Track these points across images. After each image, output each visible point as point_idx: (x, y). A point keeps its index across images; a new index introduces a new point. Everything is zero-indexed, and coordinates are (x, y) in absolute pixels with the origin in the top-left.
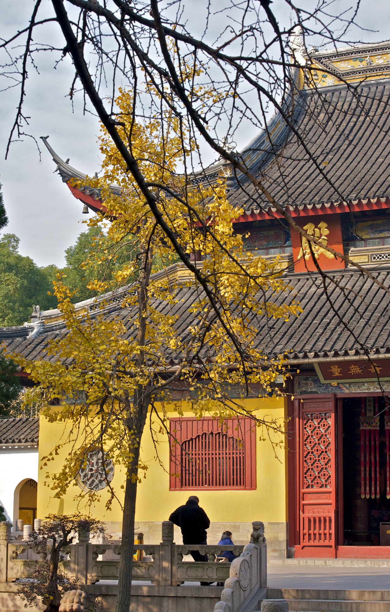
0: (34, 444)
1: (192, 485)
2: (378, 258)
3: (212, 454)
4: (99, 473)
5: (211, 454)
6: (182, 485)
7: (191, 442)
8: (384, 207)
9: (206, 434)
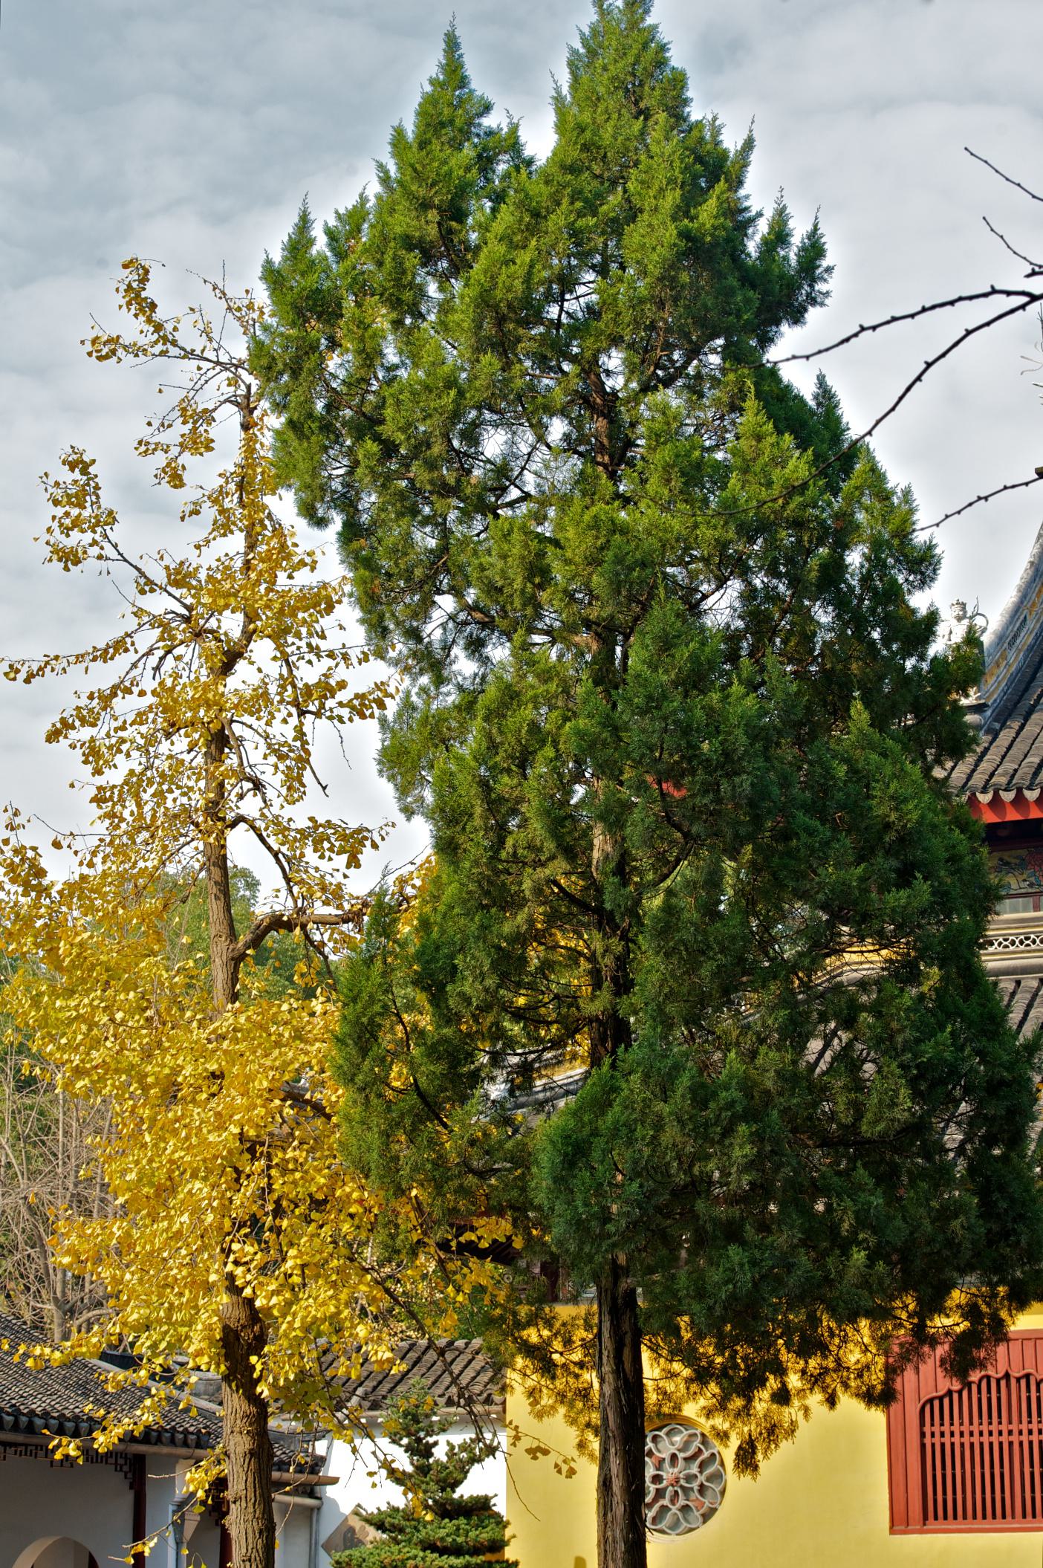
0: (494, 1408)
1: (1024, 1516)
2: (1021, 942)
3: (1010, 1432)
4: (682, 1487)
5: (1005, 1433)
6: (925, 1518)
7: (946, 1401)
8: (1035, 814)
9: (988, 1377)
